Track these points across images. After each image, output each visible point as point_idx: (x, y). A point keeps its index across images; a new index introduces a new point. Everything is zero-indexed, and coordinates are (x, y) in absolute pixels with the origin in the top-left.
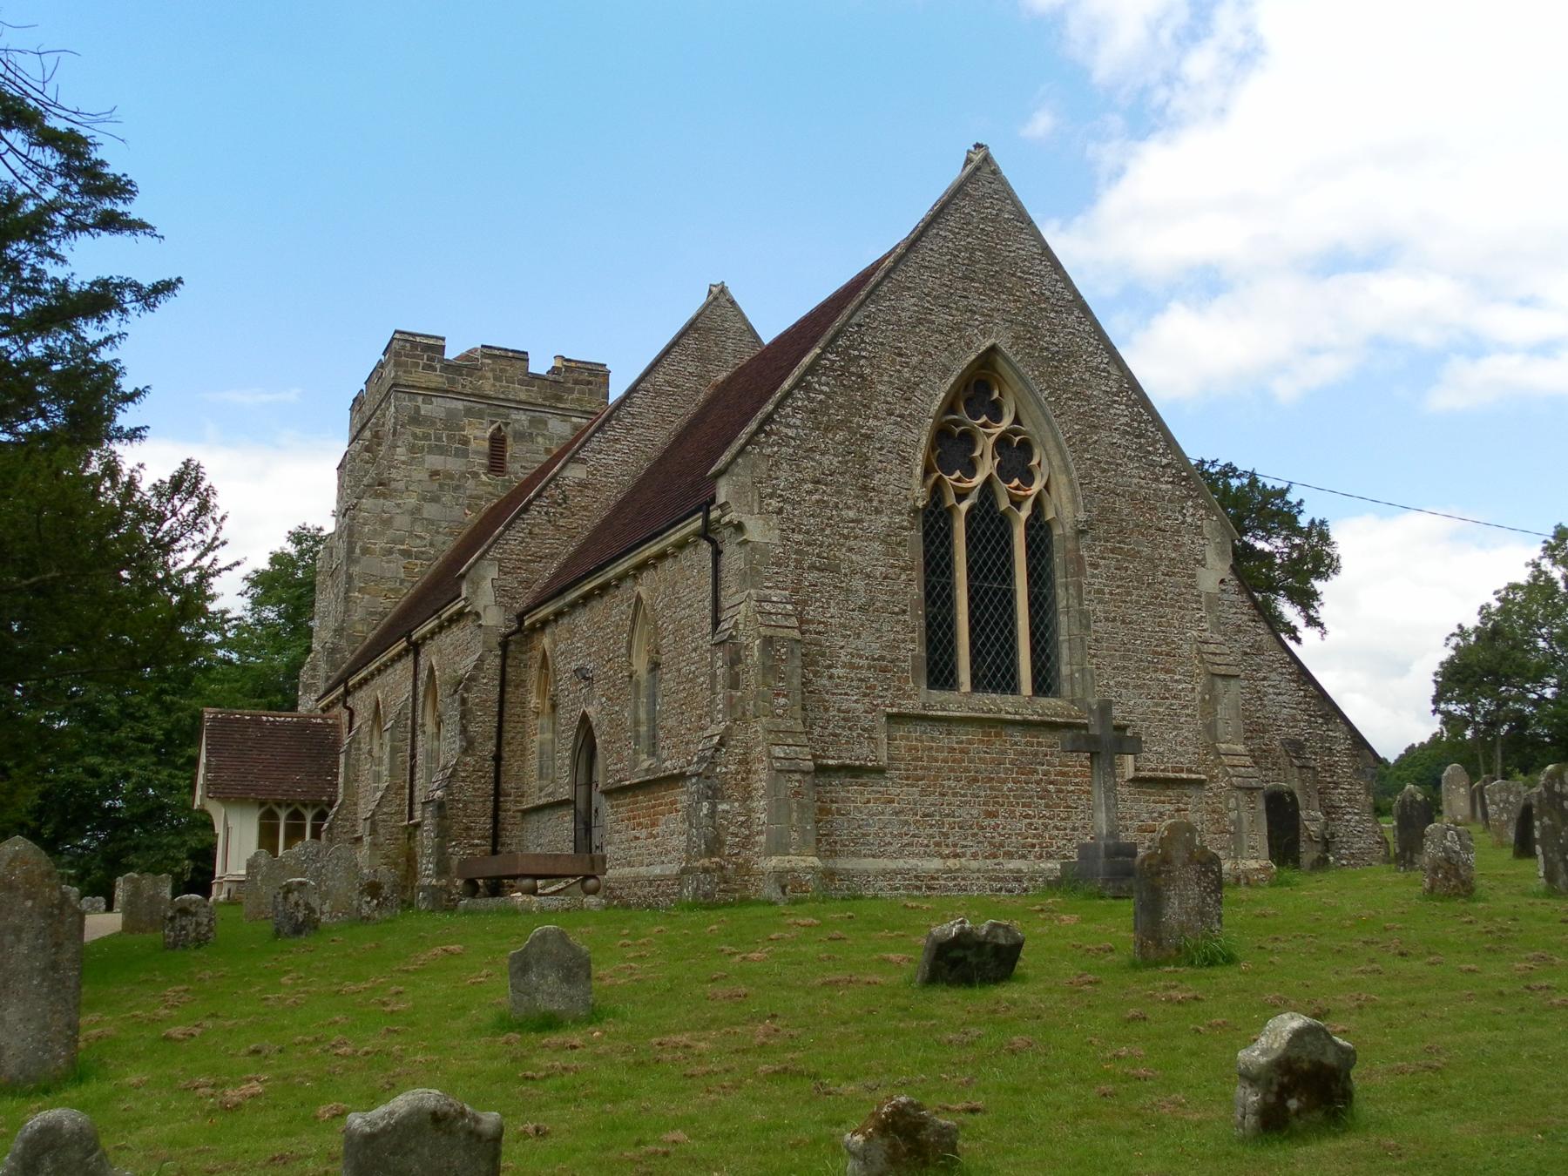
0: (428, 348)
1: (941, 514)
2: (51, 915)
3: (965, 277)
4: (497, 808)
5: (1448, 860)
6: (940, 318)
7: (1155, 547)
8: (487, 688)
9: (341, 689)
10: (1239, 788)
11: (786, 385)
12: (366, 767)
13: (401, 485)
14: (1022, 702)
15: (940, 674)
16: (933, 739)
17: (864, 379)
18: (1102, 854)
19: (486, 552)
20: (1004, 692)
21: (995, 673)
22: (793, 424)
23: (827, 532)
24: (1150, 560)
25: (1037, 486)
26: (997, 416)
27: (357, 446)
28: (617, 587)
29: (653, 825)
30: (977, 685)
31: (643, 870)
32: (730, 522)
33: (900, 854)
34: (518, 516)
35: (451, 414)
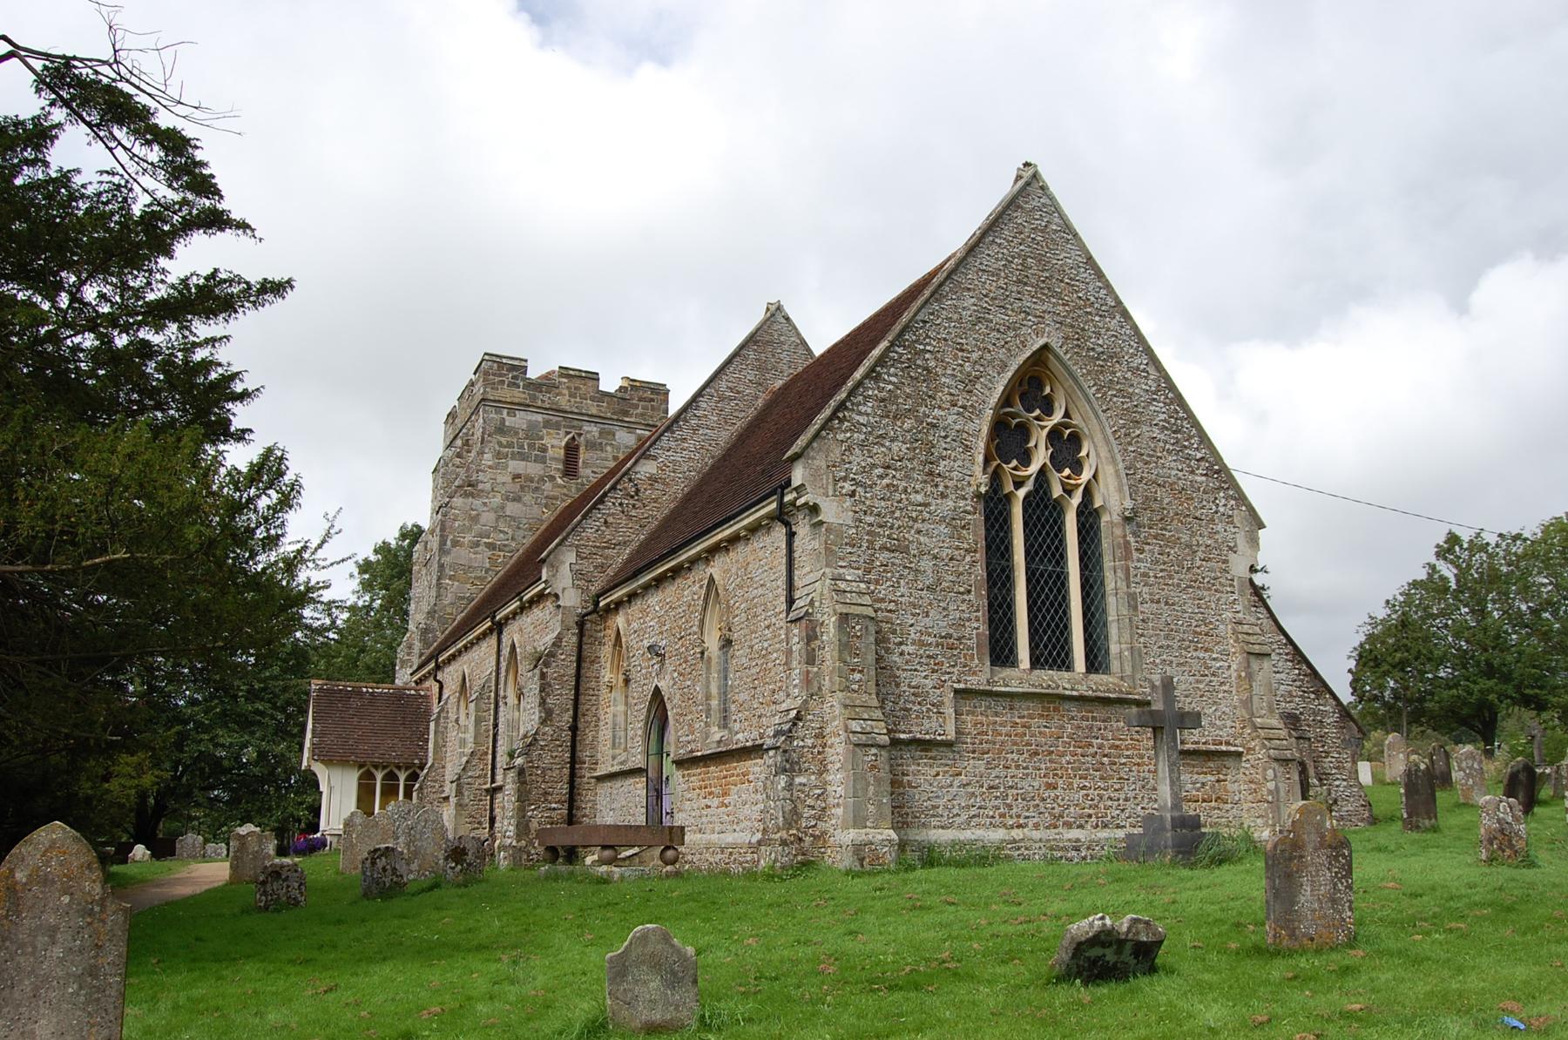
0: (514, 368)
1: (1000, 500)
2: (91, 913)
3: (1019, 281)
4: (573, 775)
5: (1502, 831)
6: (998, 318)
7: (1193, 535)
8: (565, 664)
9: (432, 665)
10: (1276, 760)
11: (858, 375)
12: (452, 734)
13: (488, 486)
14: (1076, 677)
15: (1002, 653)
16: (996, 714)
17: (929, 372)
18: (1169, 826)
19: (565, 539)
20: (1059, 668)
21: (1051, 652)
22: (865, 412)
23: (897, 514)
24: (1189, 546)
25: (1086, 476)
26: (1049, 411)
27: (450, 453)
28: (689, 569)
29: (725, 794)
30: (1036, 662)
31: (714, 837)
32: (806, 503)
33: (967, 825)
34: (594, 507)
35: (532, 426)
